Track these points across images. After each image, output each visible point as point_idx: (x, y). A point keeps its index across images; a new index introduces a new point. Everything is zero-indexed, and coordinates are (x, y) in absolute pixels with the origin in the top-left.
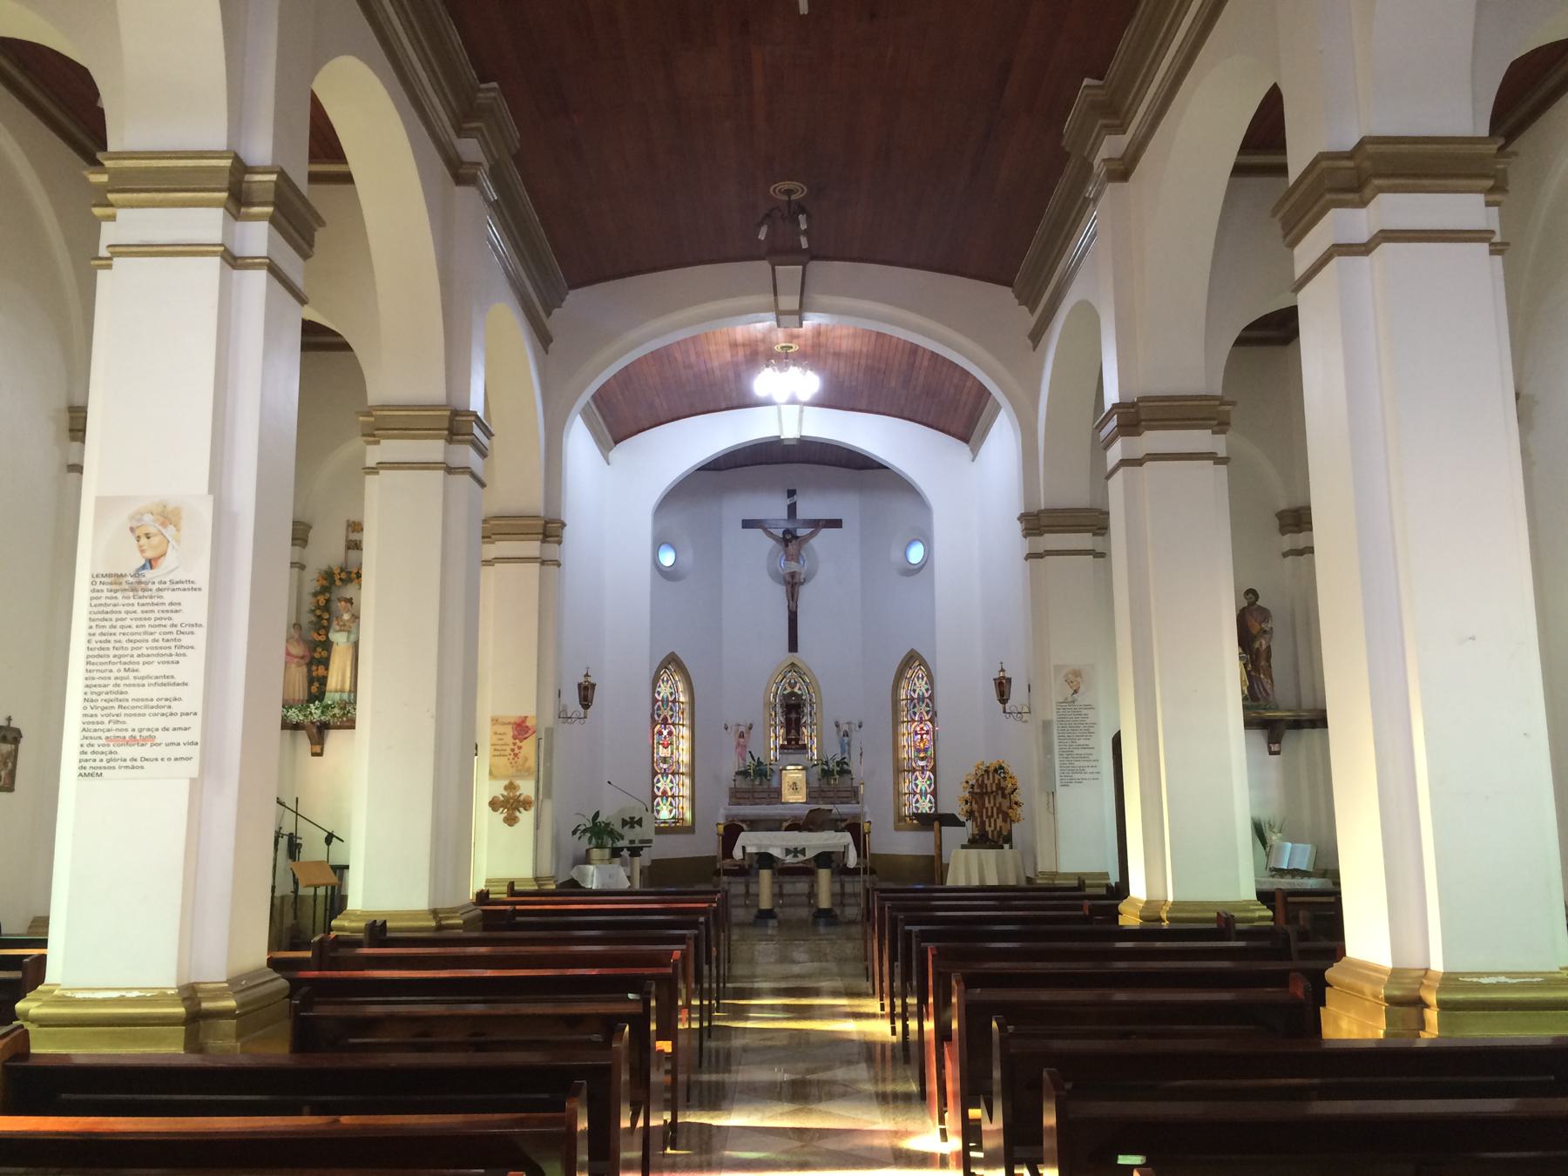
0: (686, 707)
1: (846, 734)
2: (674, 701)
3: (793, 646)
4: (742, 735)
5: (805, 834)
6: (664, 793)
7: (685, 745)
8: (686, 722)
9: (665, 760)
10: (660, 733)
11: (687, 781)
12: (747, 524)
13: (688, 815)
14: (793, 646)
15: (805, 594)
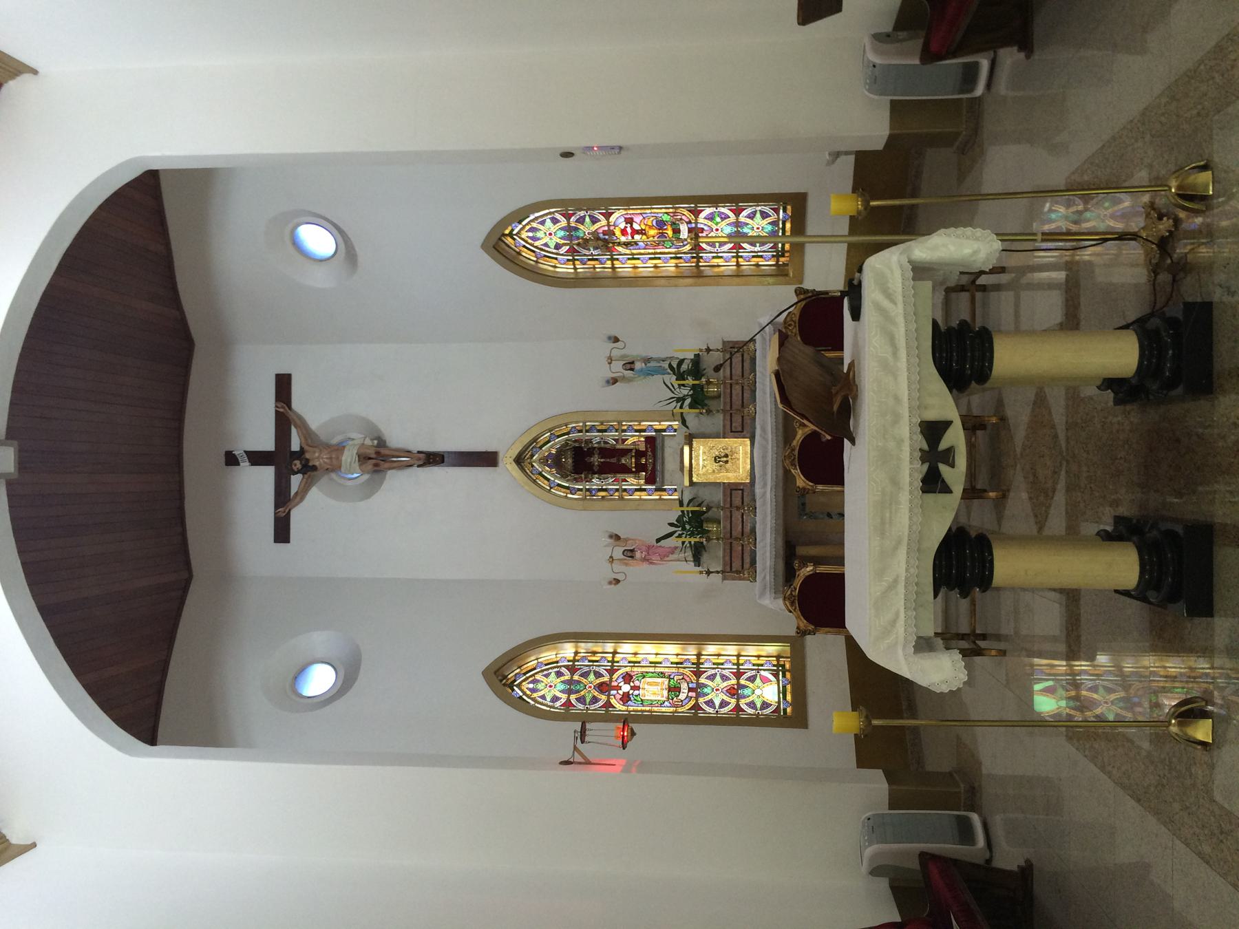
0: (583, 647)
1: (630, 365)
2: (572, 669)
3: (487, 459)
4: (630, 554)
6: (732, 692)
7: (648, 650)
8: (609, 647)
9: (674, 690)
10: (626, 698)
11: (711, 649)
12: (282, 533)
13: (772, 649)
14: (487, 459)
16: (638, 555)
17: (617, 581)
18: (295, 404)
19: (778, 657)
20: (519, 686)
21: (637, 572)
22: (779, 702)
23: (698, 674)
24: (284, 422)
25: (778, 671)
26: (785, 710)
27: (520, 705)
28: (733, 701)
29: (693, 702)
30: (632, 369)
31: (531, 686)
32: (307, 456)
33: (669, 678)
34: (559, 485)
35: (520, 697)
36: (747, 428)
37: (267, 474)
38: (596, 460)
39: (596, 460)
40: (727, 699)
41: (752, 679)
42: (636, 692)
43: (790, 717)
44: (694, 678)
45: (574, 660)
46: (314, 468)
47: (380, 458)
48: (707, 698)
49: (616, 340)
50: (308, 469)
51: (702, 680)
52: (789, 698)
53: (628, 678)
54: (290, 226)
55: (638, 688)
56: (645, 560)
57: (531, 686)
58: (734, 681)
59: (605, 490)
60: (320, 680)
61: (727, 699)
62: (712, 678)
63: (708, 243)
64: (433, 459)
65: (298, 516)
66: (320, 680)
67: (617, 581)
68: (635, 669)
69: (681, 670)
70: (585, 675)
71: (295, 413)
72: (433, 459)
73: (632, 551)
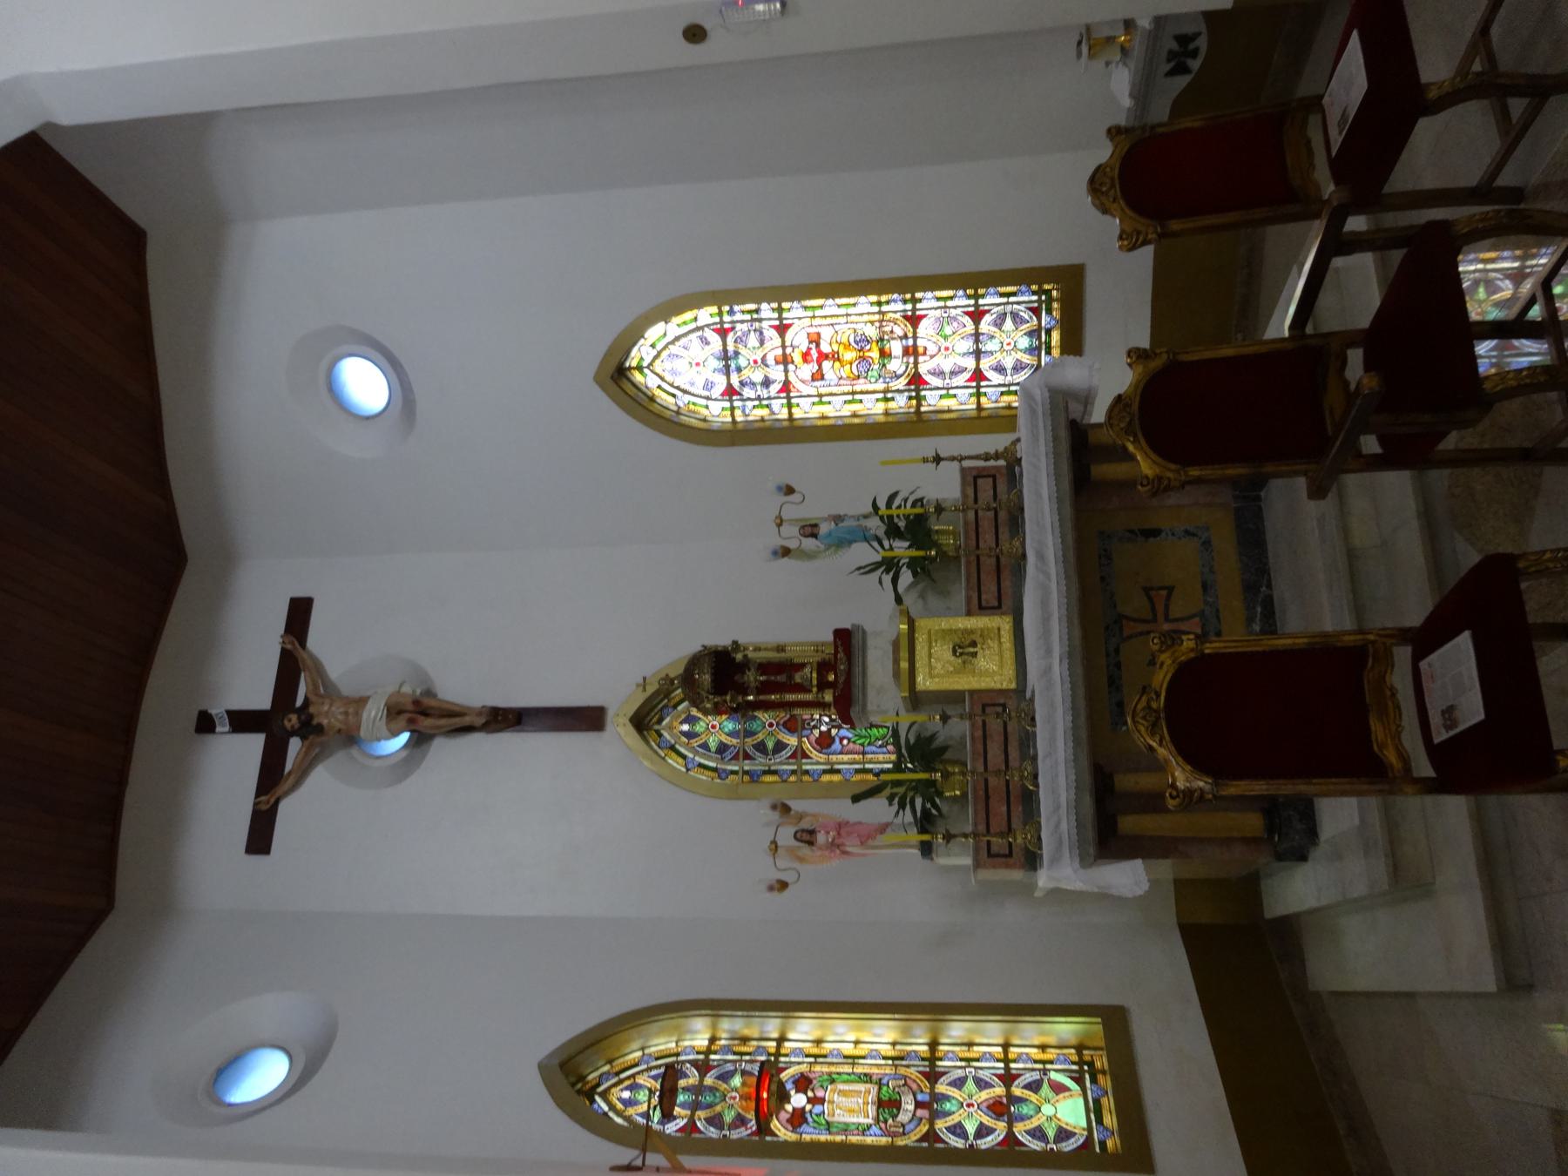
0: (729, 1026)
1: (810, 530)
3: (588, 719)
4: (807, 837)
5: (1313, 144)
6: (998, 1109)
7: (843, 1034)
8: (772, 1027)
9: (887, 1105)
10: (798, 1119)
11: (957, 1029)
12: (260, 838)
13: (1065, 1029)
14: (588, 719)
15: (465, 688)
16: (821, 838)
17: (783, 885)
18: (313, 641)
19: (1080, 1048)
20: (604, 1095)
21: (817, 869)
22: (1090, 1128)
23: (933, 1076)
24: (290, 667)
25: (1081, 1072)
26: (1103, 1144)
27: (600, 1126)
28: (1001, 1126)
29: (924, 1128)
30: (814, 536)
31: (626, 1095)
32: (312, 710)
33: (880, 1083)
34: (701, 765)
35: (605, 1114)
36: (1008, 603)
37: (254, 744)
38: (751, 677)
39: (751, 677)
40: (988, 1121)
41: (1034, 1087)
42: (818, 1109)
43: (1115, 1155)
44: (925, 1085)
45: (708, 1051)
46: (320, 730)
47: (427, 717)
48: (951, 1121)
49: (790, 490)
50: (309, 728)
51: (941, 1088)
52: (1110, 1120)
53: (803, 1083)
54: (324, 365)
55: (822, 1101)
56: (834, 846)
57: (626, 1095)
58: (999, 1090)
59: (775, 772)
60: (265, 1074)
61: (988, 1121)
62: (959, 1083)
63: (933, 373)
64: (504, 719)
65: (290, 811)
66: (265, 1074)
67: (783, 885)
68: (818, 1068)
69: (902, 1071)
70: (725, 1077)
71: (312, 656)
72: (504, 719)
73: (812, 832)
